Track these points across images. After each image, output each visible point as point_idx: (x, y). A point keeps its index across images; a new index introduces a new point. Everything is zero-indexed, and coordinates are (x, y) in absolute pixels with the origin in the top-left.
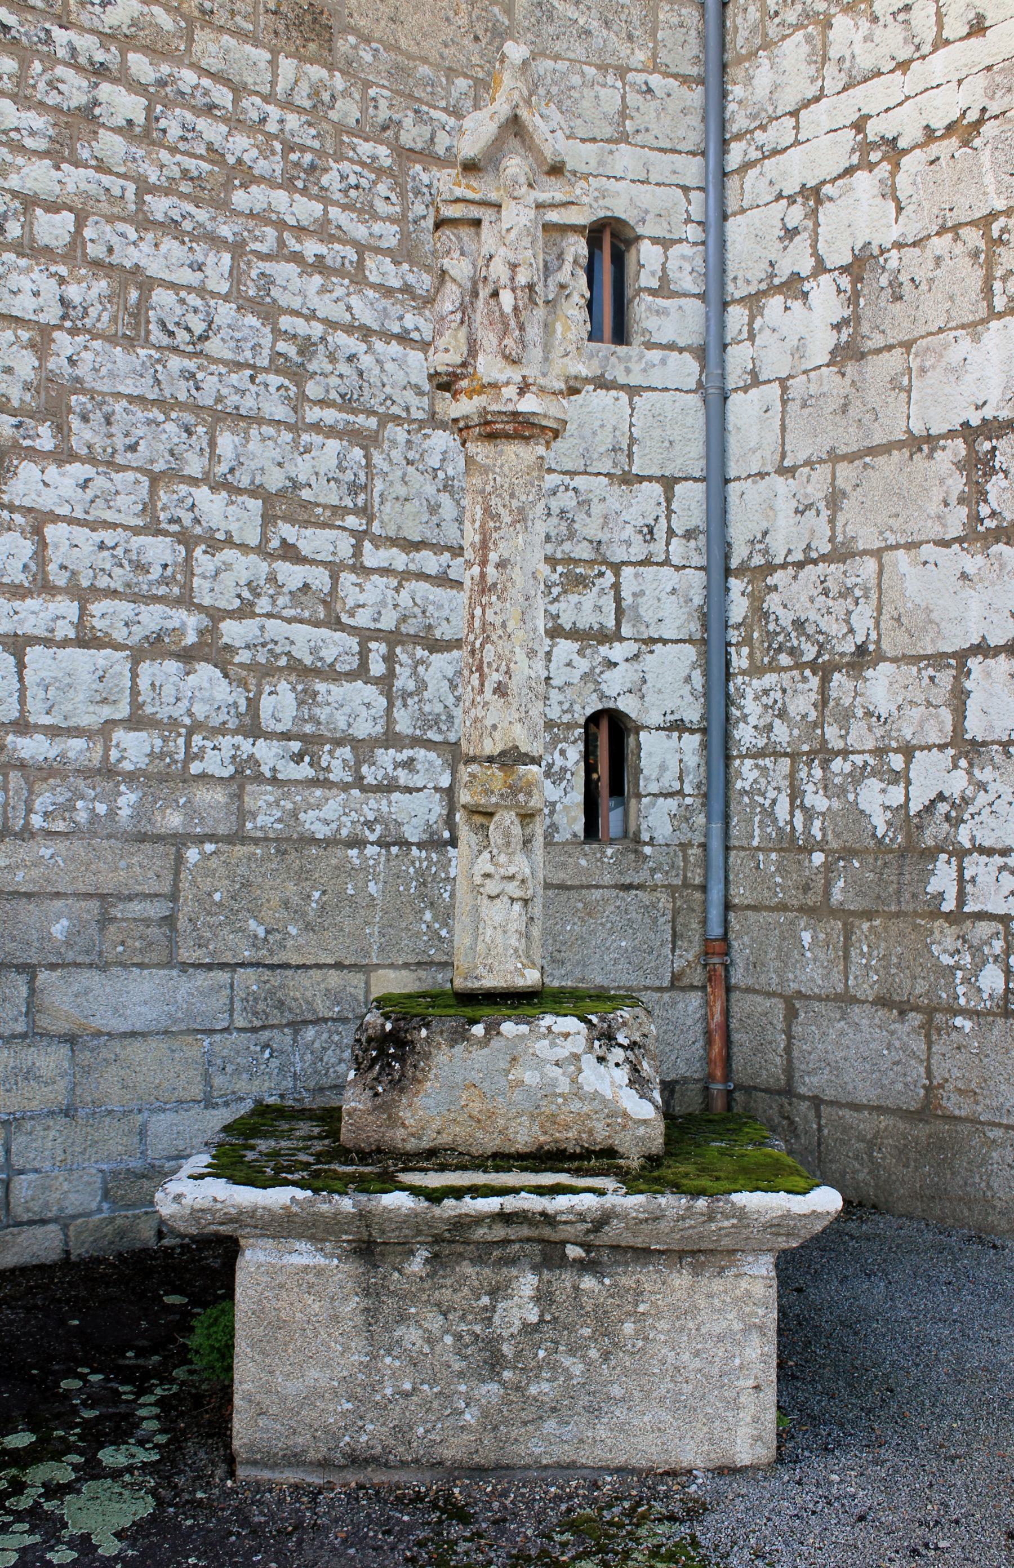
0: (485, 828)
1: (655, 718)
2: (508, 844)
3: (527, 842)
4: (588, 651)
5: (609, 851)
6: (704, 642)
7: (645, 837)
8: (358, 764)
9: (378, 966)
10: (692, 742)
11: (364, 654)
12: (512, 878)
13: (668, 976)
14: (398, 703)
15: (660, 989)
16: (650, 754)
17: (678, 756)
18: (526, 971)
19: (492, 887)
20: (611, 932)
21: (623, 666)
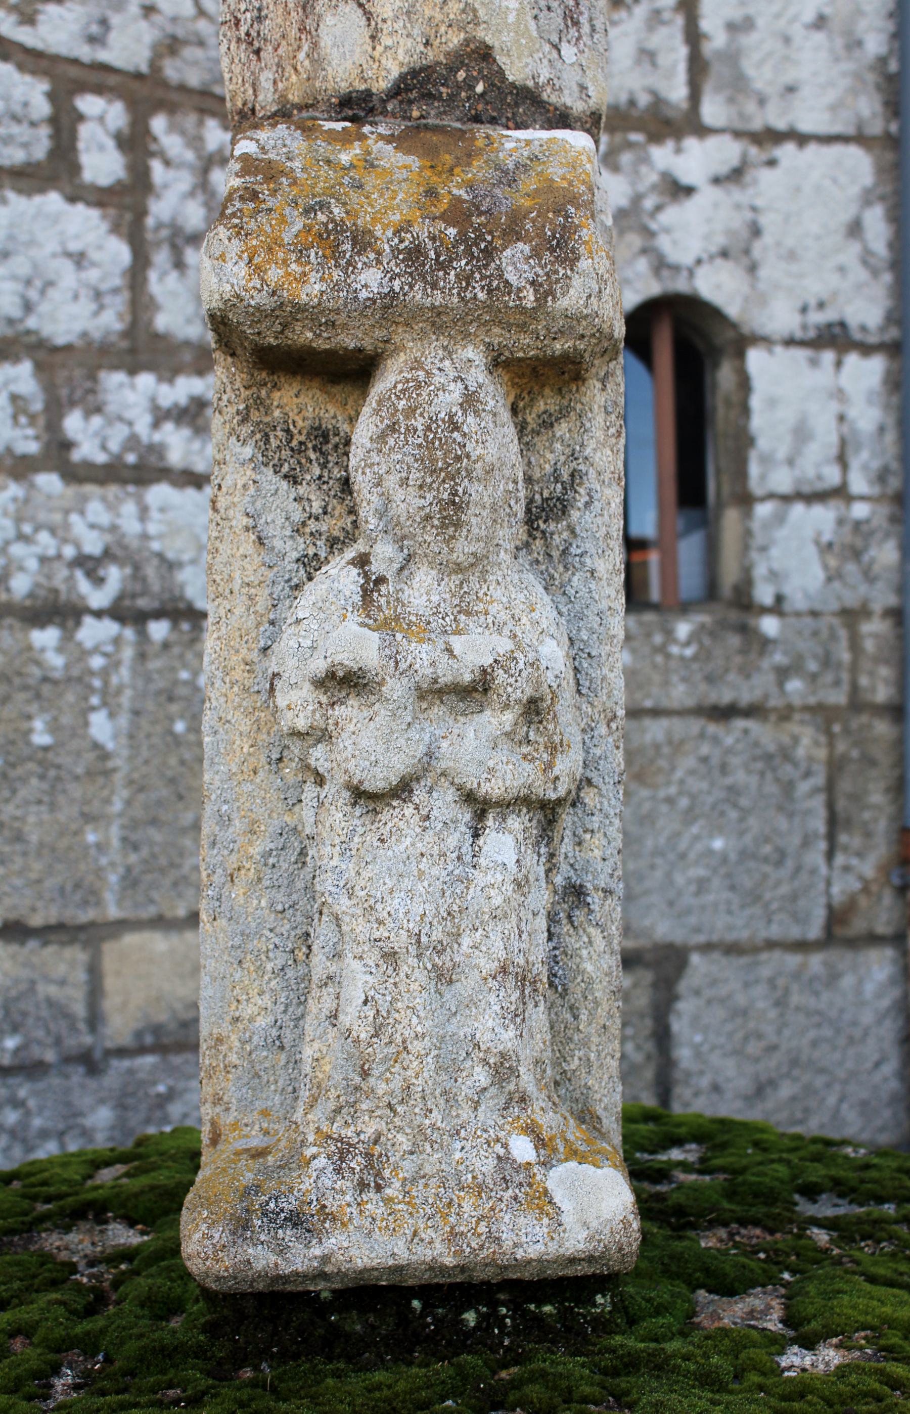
0: (328, 443)
1: (780, 318)
2: (451, 514)
3: (546, 512)
4: (626, 158)
5: (683, 629)
6: (892, 142)
7: (764, 594)
8: (55, 410)
9: (122, 926)
10: (865, 374)
11: (64, 125)
12: (475, 692)
13: (819, 916)
14: (161, 257)
15: (801, 946)
16: (772, 403)
17: (834, 407)
18: (561, 1180)
19: (369, 743)
20: (690, 816)
21: (707, 195)
